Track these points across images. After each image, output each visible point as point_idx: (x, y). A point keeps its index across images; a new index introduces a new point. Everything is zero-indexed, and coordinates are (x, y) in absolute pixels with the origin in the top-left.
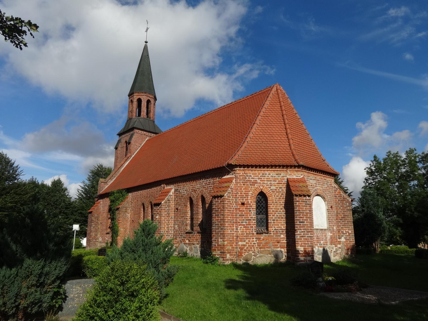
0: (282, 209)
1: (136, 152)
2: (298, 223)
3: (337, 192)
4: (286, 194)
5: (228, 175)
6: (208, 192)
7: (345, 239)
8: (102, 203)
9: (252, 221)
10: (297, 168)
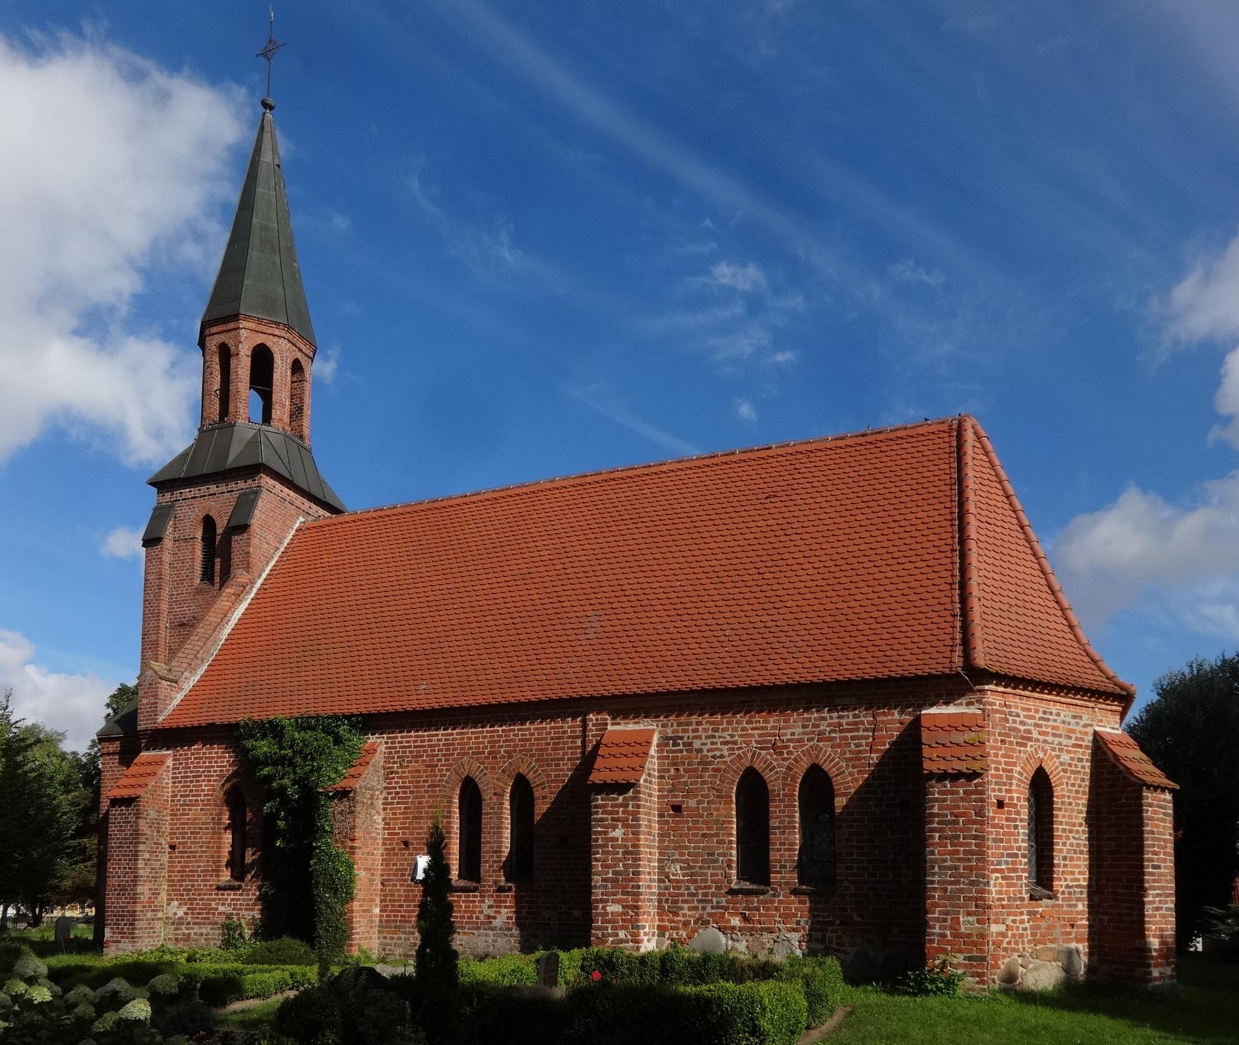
0: (1081, 825)
1: (267, 571)
4: (1091, 780)
5: (947, 703)
6: (848, 755)
8: (170, 762)
9: (1020, 859)
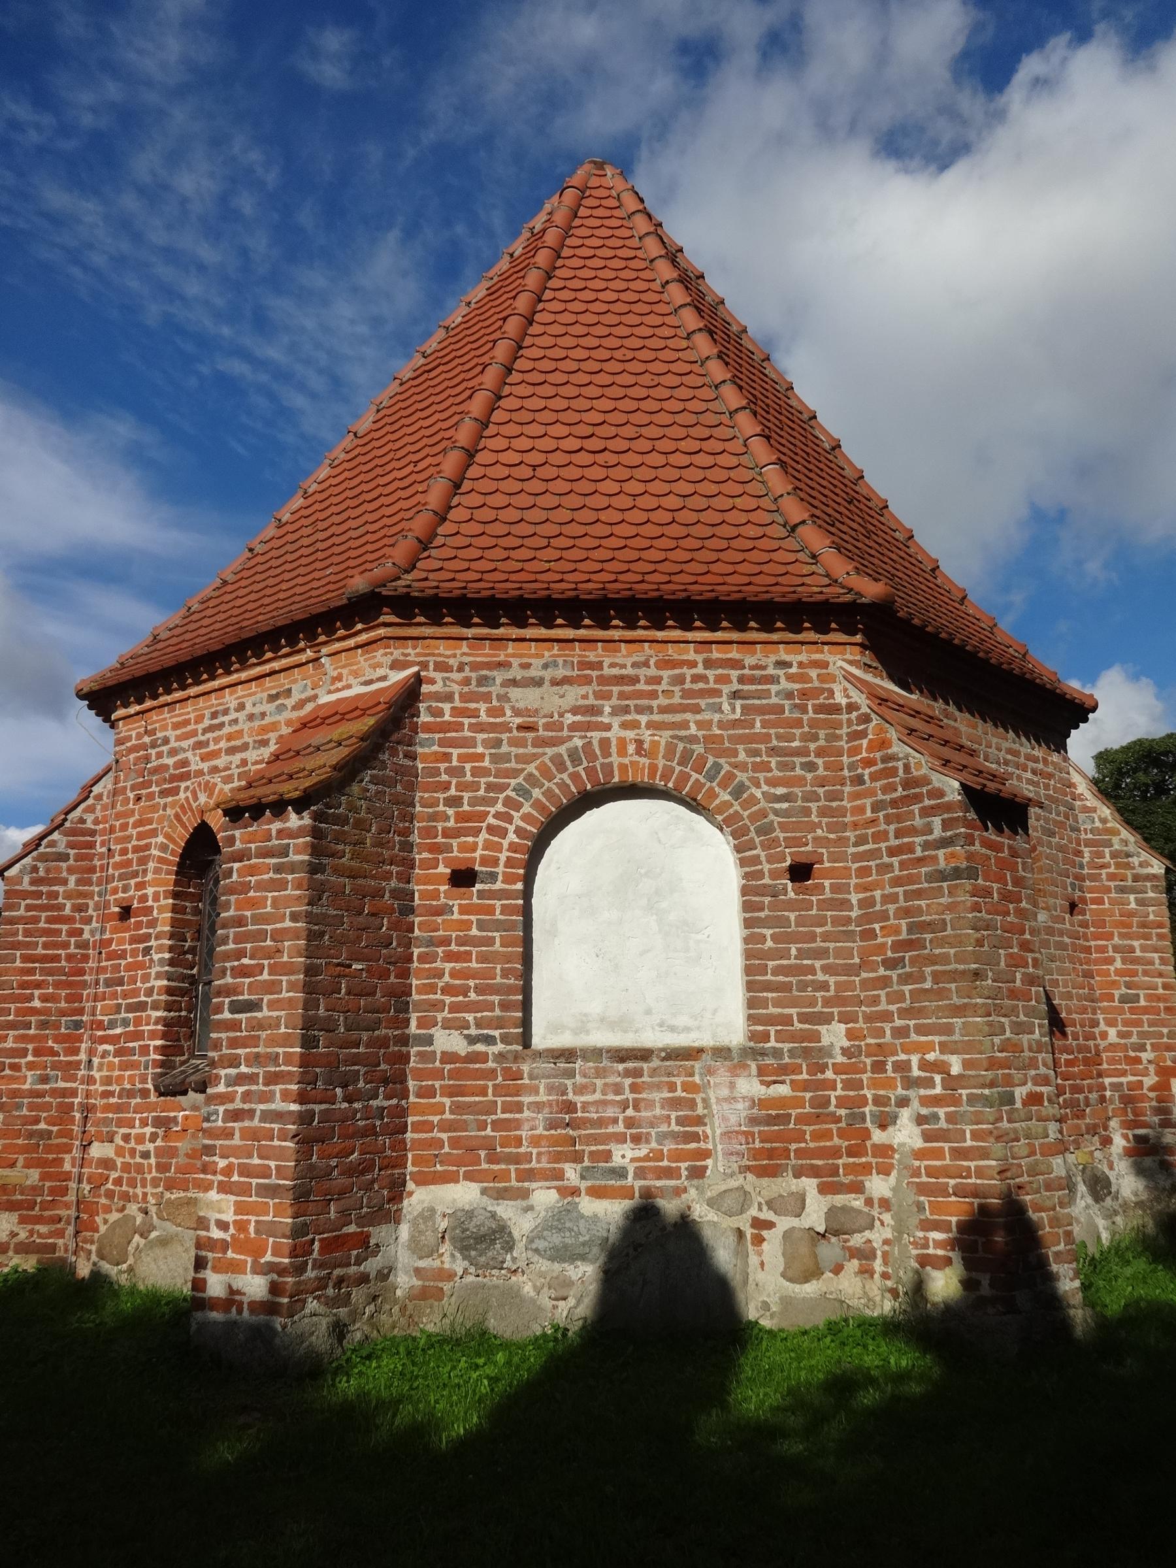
2: (227, 1015)
3: (865, 742)
7: (917, 1131)
10: (359, 626)
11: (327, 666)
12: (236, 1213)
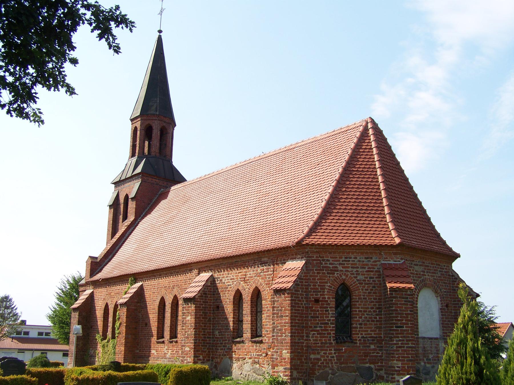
11: (383, 255)
12: (401, 365)
